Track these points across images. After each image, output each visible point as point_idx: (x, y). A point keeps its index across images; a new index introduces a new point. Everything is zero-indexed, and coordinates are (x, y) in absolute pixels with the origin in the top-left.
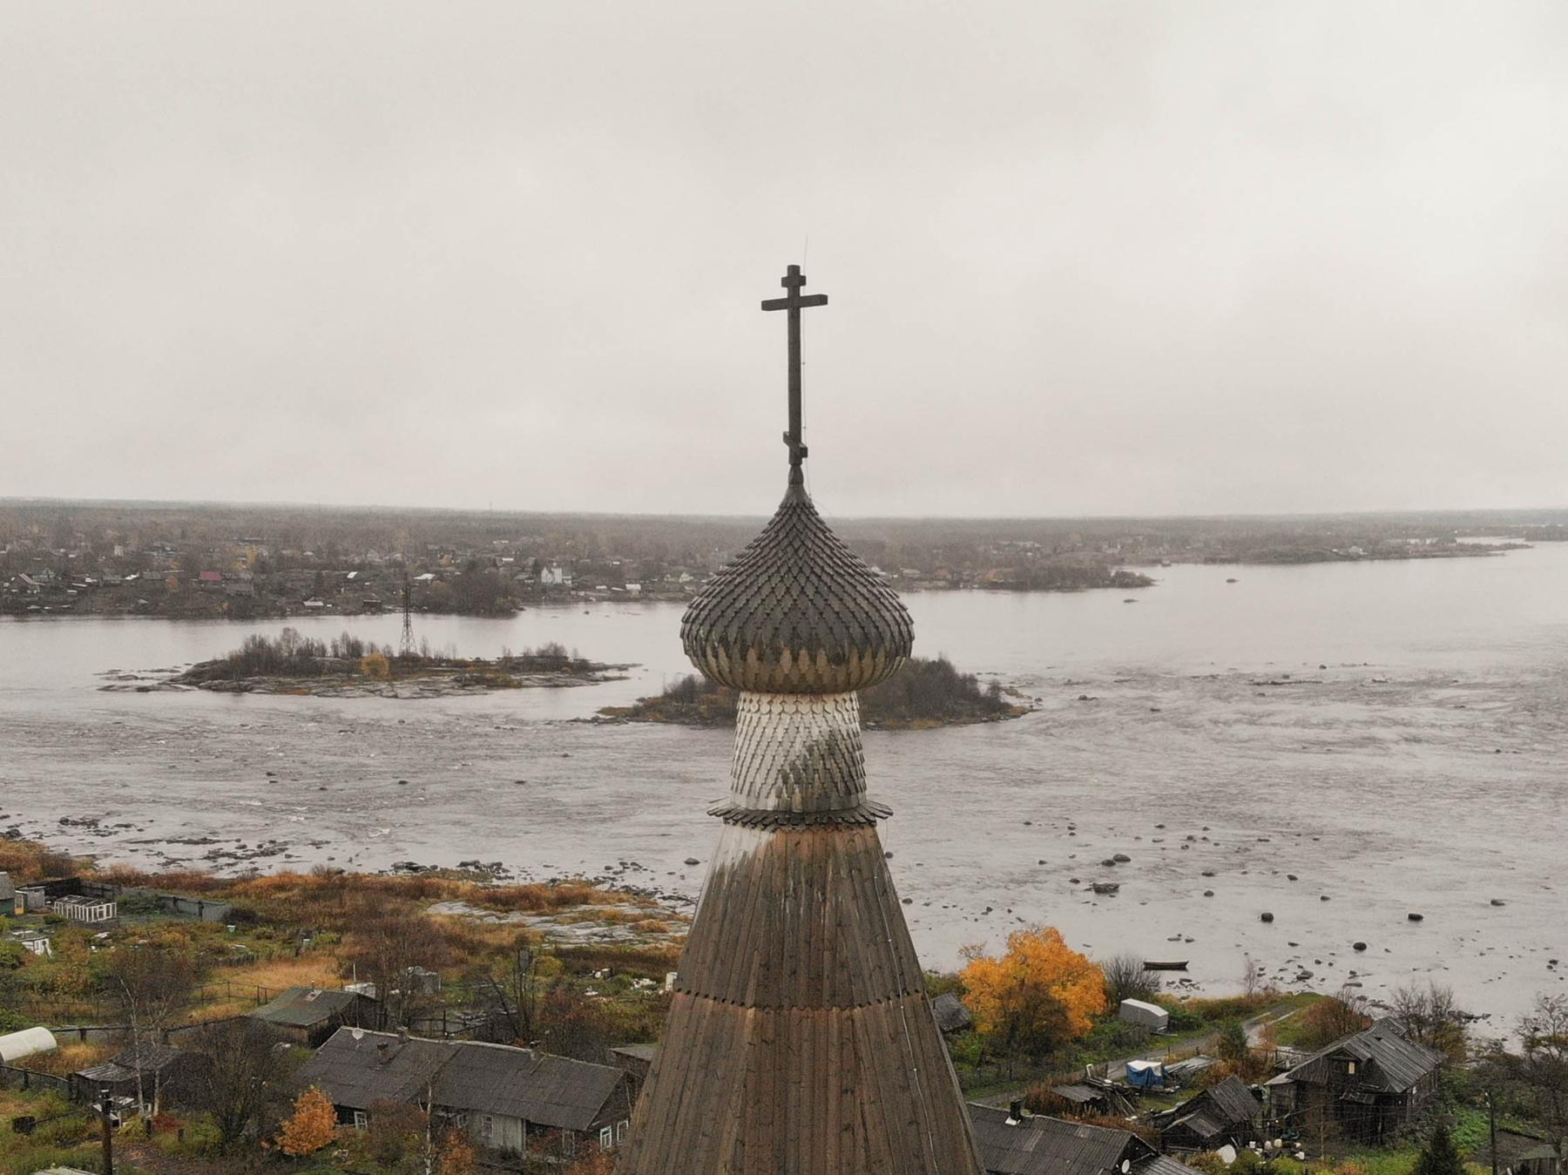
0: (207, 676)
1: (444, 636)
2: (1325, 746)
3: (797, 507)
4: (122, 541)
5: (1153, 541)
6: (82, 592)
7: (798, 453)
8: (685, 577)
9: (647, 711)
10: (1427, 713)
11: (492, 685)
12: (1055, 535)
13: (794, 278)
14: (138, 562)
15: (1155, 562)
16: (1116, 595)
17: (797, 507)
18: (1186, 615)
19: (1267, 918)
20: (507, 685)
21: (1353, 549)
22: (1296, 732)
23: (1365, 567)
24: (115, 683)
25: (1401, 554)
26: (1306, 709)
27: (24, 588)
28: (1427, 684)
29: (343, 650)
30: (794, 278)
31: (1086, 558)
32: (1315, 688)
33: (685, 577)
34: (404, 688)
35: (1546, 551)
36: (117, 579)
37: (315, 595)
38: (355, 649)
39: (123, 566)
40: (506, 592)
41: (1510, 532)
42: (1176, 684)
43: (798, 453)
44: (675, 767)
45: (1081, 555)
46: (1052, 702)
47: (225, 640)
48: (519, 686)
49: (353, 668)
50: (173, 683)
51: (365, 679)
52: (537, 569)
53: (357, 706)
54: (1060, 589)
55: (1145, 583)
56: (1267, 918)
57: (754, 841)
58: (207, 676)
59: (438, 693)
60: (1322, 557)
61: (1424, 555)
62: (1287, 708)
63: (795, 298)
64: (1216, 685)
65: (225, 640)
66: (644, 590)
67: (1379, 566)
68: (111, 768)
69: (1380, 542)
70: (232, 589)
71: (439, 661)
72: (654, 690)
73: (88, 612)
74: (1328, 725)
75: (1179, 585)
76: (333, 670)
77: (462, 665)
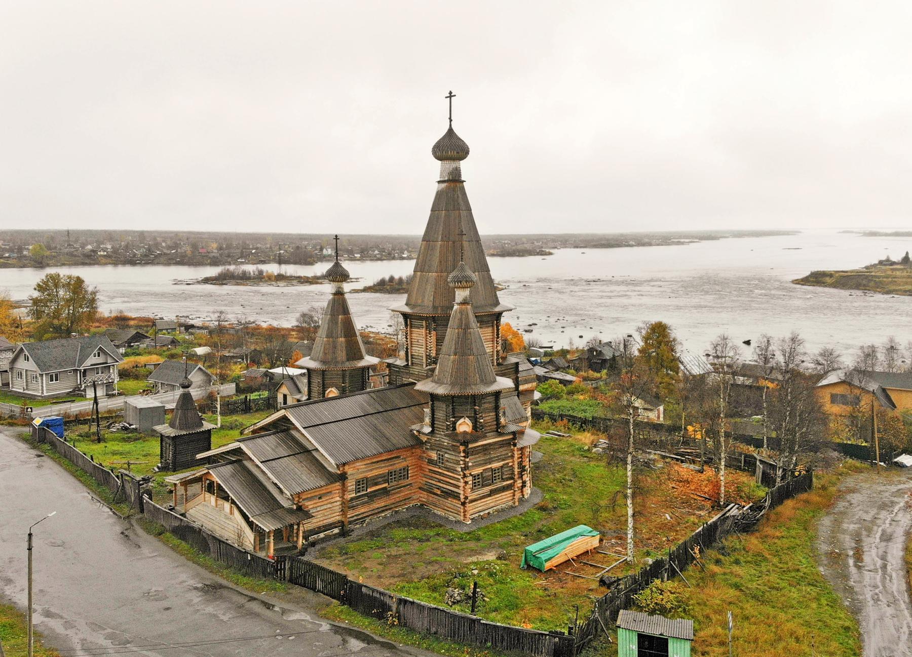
0: (206, 281)
1: (290, 270)
2: (610, 297)
3: (451, 131)
4: (164, 241)
5: (554, 241)
6: (156, 256)
7: (451, 120)
8: (376, 252)
9: (366, 290)
10: (649, 288)
11: (311, 283)
12: (516, 240)
13: (451, 93)
14: (176, 246)
15: (555, 248)
16: (539, 258)
17: (451, 131)
18: (564, 262)
19: (581, 337)
20: (317, 283)
21: (631, 243)
22: (600, 294)
23: (635, 248)
24: (177, 283)
25: (650, 244)
26: (604, 288)
27: (135, 255)
28: (649, 281)
29: (257, 273)
30: (451, 93)
31: (528, 246)
32: (609, 282)
33: (376, 252)
34: (281, 284)
35: (705, 243)
36: (168, 252)
37: (241, 257)
38: (261, 272)
39: (169, 248)
40: (311, 257)
41: (696, 238)
42: (558, 282)
43: (451, 120)
44: (380, 304)
45: (526, 246)
46: (513, 287)
47: (213, 271)
48: (321, 283)
49: (260, 278)
50: (199, 282)
51: (266, 281)
52: (321, 249)
53: (265, 288)
54: (518, 256)
55: (550, 254)
56: (581, 337)
57: (444, 185)
58: (206, 281)
59: (293, 285)
60: (619, 246)
61: (658, 245)
62: (596, 288)
63: (451, 96)
64: (572, 282)
65: (213, 271)
66: (362, 256)
67: (641, 248)
68: (187, 304)
69: (641, 241)
70: (211, 255)
71: (291, 277)
72: (370, 283)
73: (158, 264)
74: (611, 292)
75: (562, 255)
76: (254, 278)
77: (299, 277)
